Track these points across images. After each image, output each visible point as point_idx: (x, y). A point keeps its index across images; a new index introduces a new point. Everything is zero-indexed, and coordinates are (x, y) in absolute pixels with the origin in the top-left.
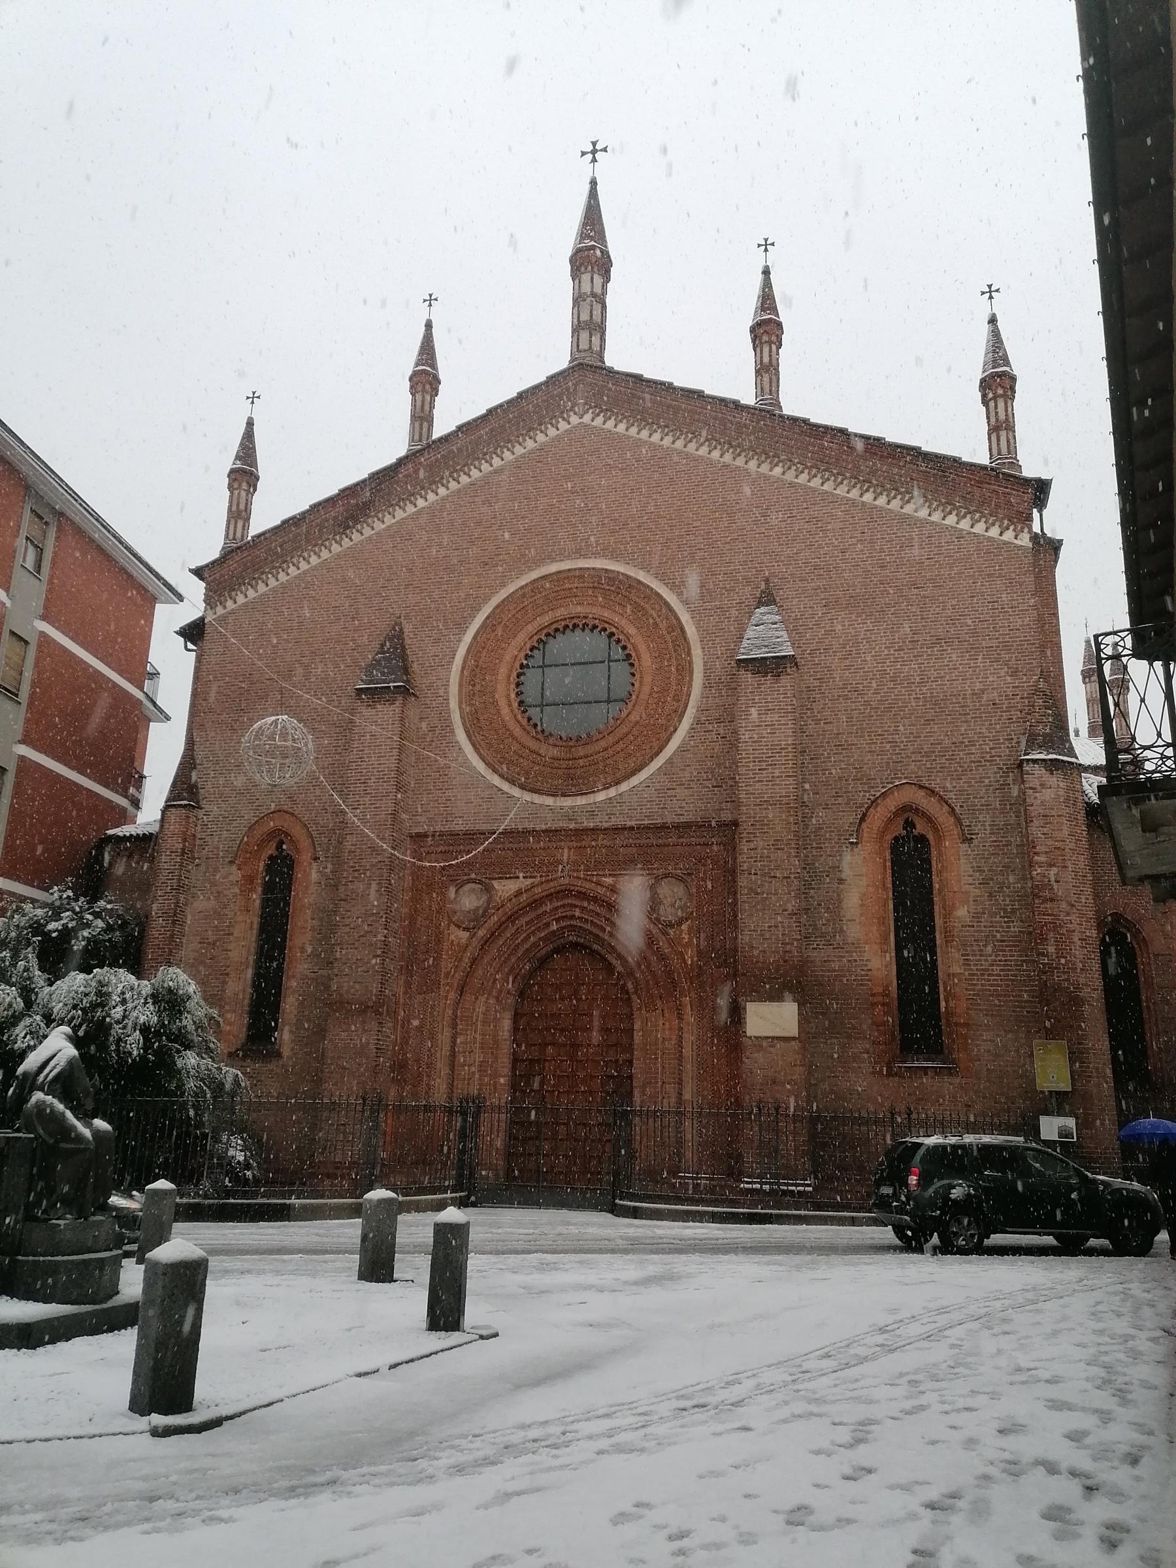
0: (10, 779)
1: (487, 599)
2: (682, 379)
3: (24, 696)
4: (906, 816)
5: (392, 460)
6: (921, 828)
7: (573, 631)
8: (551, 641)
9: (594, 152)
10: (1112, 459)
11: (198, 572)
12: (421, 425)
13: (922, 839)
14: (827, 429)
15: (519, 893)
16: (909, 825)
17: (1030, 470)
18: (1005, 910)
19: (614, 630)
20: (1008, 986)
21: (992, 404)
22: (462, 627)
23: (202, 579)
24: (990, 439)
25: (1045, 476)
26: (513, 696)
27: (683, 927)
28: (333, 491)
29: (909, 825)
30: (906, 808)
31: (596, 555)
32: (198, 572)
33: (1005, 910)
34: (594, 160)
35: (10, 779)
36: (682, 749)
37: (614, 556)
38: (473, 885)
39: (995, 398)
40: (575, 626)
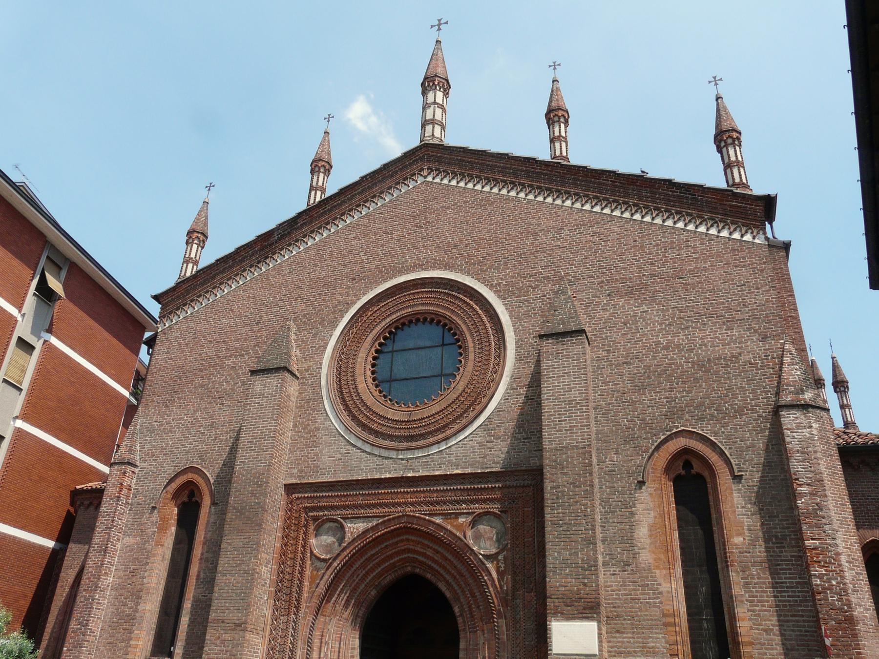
0: (6, 444)
1: (354, 303)
2: (494, 148)
3: (25, 386)
4: (687, 457)
5: (292, 214)
6: (697, 467)
7: (416, 324)
8: (399, 332)
9: (439, 25)
10: (858, 176)
11: (157, 298)
12: (739, 170)
13: (699, 477)
14: (603, 172)
15: (366, 532)
16: (687, 465)
17: (758, 189)
18: (776, 537)
19: (447, 321)
20: (785, 606)
21: (724, 150)
22: (334, 326)
23: (160, 303)
24: (310, 193)
25: (772, 193)
26: (369, 373)
27: (500, 557)
28: (252, 237)
29: (687, 465)
30: (686, 451)
31: (433, 267)
32: (157, 298)
33: (776, 537)
34: (439, 29)
35: (6, 444)
36: (498, 410)
37: (448, 267)
38: (331, 524)
39: (726, 146)
40: (418, 320)
